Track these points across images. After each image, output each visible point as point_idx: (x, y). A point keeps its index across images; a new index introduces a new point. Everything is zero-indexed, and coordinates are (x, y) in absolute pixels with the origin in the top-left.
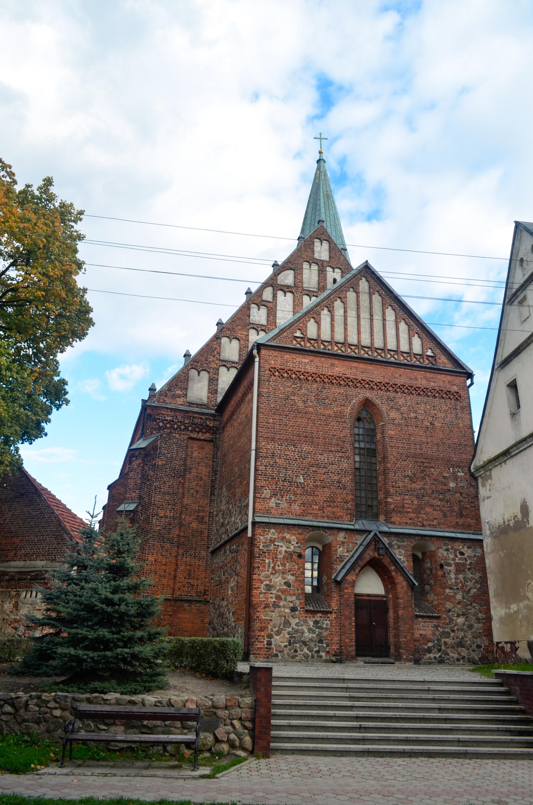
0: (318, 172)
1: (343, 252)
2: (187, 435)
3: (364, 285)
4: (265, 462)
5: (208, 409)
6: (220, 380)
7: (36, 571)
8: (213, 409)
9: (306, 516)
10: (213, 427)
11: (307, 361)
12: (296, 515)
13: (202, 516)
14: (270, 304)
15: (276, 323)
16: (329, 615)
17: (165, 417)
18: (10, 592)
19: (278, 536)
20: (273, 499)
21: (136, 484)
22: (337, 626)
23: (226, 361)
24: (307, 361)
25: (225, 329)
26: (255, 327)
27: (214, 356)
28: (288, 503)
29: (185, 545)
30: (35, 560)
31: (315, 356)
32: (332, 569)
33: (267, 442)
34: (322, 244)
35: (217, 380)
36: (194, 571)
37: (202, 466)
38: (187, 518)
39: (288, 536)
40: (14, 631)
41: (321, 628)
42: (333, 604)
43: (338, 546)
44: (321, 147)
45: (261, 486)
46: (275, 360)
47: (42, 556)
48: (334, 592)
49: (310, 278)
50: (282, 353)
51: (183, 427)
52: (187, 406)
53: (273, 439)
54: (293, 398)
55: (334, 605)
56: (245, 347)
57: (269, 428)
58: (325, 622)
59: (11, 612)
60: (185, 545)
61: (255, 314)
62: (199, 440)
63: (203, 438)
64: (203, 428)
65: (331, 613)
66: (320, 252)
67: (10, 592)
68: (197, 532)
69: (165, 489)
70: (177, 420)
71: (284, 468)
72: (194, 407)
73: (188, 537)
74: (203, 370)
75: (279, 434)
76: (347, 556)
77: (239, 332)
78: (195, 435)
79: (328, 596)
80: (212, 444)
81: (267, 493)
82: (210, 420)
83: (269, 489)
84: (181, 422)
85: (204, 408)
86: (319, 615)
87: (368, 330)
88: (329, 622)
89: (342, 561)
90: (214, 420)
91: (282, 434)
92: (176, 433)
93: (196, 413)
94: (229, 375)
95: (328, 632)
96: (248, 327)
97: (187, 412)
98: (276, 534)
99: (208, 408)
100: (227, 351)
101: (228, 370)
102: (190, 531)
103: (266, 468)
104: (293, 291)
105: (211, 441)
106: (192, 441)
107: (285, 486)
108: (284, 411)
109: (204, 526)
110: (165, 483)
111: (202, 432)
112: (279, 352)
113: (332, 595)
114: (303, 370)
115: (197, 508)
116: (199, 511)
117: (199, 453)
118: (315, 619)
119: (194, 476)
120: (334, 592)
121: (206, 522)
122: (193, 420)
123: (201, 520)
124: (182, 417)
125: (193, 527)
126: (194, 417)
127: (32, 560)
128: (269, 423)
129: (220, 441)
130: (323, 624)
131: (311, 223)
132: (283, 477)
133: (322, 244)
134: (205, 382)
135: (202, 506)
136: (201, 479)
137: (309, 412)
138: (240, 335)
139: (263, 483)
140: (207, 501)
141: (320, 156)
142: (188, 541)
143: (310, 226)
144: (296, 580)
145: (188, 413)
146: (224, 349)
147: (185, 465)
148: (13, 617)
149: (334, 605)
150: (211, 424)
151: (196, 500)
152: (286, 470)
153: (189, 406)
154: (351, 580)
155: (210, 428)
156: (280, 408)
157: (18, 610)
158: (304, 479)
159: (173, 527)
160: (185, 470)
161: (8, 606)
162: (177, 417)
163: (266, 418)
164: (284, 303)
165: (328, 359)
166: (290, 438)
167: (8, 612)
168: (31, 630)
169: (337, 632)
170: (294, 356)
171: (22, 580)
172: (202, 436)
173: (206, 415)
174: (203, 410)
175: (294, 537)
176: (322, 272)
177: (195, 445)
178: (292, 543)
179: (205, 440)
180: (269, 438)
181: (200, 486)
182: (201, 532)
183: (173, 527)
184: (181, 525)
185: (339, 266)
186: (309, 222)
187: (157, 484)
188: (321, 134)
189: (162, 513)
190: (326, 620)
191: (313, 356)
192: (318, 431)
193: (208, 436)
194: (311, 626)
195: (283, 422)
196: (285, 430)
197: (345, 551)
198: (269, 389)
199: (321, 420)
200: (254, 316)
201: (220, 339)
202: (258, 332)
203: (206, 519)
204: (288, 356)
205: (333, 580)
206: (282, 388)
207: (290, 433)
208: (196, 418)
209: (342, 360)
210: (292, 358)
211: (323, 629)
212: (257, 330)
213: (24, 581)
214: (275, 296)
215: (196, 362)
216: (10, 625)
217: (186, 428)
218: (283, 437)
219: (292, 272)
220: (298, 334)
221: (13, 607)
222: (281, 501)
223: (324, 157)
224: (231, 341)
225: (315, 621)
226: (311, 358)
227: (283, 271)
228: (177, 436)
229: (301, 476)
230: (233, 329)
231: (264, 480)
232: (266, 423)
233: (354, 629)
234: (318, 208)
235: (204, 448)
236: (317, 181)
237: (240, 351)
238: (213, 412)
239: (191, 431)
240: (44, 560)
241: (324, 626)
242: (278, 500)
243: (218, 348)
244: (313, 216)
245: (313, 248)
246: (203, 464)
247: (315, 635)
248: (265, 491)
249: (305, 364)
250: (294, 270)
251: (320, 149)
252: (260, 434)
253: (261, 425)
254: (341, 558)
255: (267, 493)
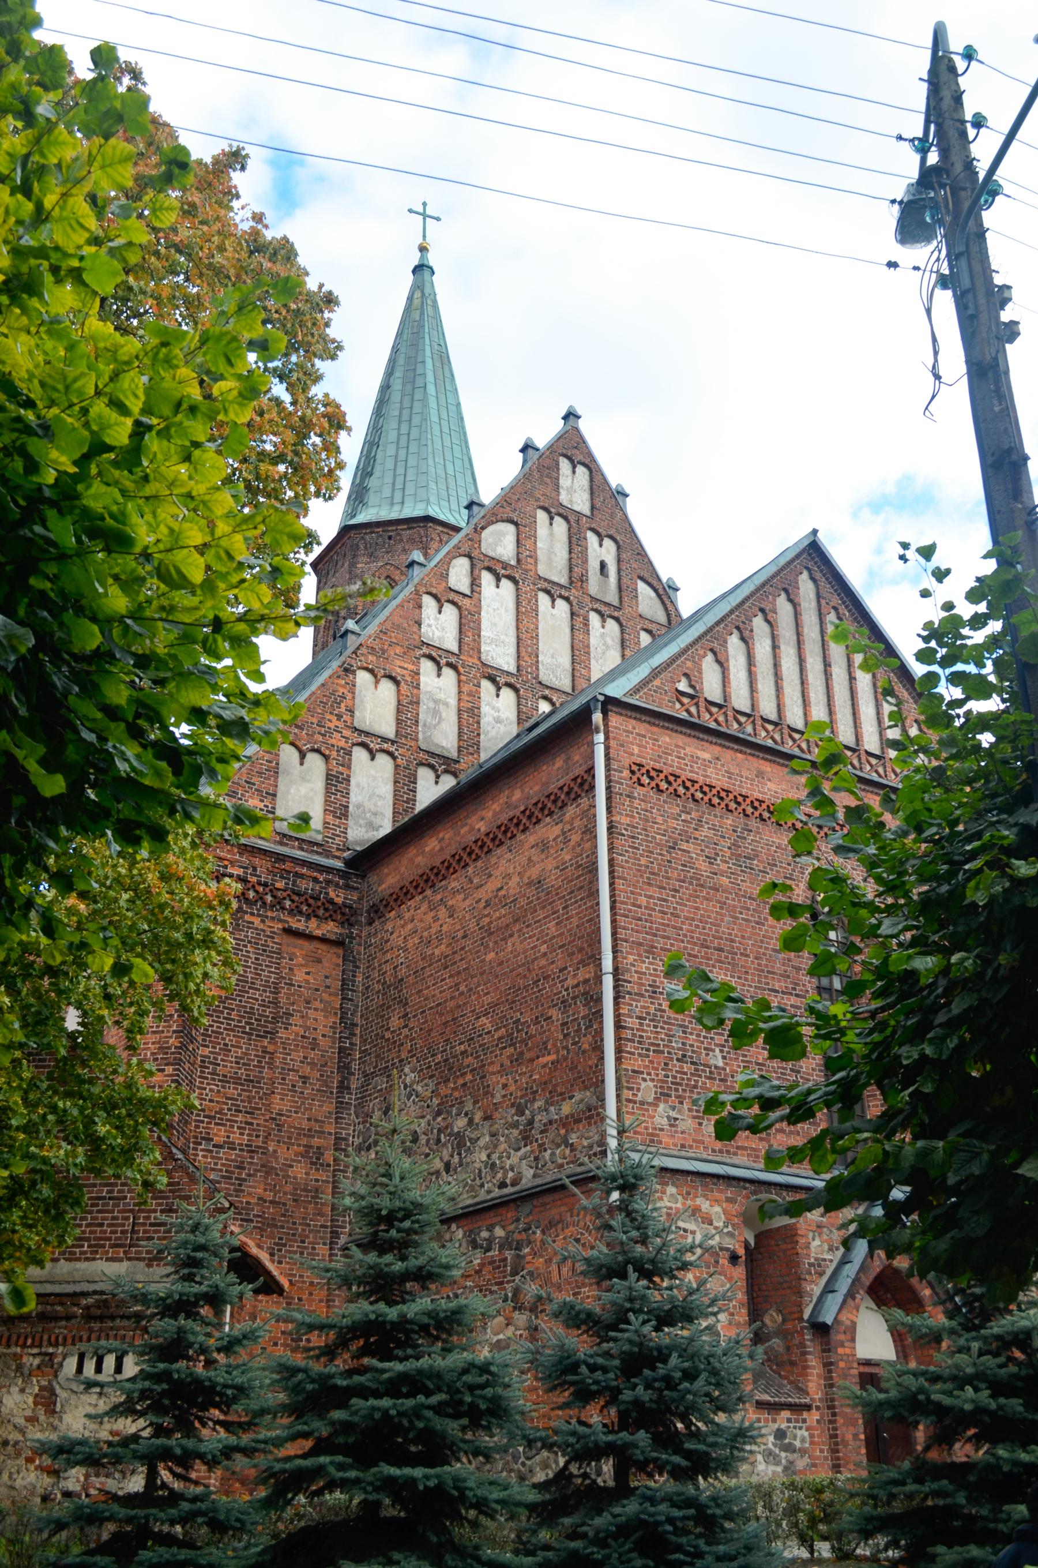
0: (418, 294)
1: (620, 498)
2: (280, 921)
3: (806, 588)
4: (639, 1006)
5: (327, 857)
6: (353, 782)
7: (95, 1292)
8: (338, 858)
9: (735, 1154)
10: (344, 905)
11: (706, 756)
12: (714, 1151)
13: (318, 1148)
14: (466, 603)
15: (479, 652)
16: (805, 1415)
17: (226, 867)
18: (17, 1357)
19: (684, 1204)
20: (662, 1106)
21: (163, 1049)
22: (823, 1443)
23: (367, 734)
24: (706, 756)
25: (363, 650)
26: (434, 654)
27: (339, 717)
28: (694, 1117)
29: (276, 1226)
30: (87, 1259)
31: (724, 746)
32: (800, 1293)
33: (640, 955)
34: (574, 472)
35: (348, 780)
36: (300, 1299)
37: (316, 1009)
38: (282, 1152)
39: (705, 1205)
40: (47, 1480)
41: (789, 1448)
42: (810, 1384)
43: (811, 1234)
44: (424, 236)
45: (634, 1071)
46: (643, 743)
47: (112, 1246)
48: (810, 1353)
49: (551, 552)
50: (655, 729)
51: (269, 898)
52: (275, 842)
53: (651, 950)
54: (684, 846)
55: (815, 1388)
56: (411, 703)
57: (640, 919)
58: (799, 1433)
59: (32, 1420)
60: (276, 1226)
61: (432, 622)
62: (310, 937)
63: (318, 933)
64: (318, 906)
65: (808, 1407)
66: (571, 490)
67: (17, 1357)
68: (305, 1190)
69: (227, 1068)
70: (255, 879)
71: (681, 1026)
72: (293, 847)
73: (284, 1204)
74: (313, 750)
75: (664, 937)
76: (831, 1261)
77: (398, 663)
78: (298, 924)
79: (793, 1363)
80: (341, 952)
81: (647, 1090)
82: (337, 885)
83: (652, 1080)
84: (266, 885)
85: (317, 853)
86: (786, 1414)
87: (823, 699)
88: (806, 1434)
89: (821, 1274)
90: (347, 887)
91: (669, 938)
92: (252, 914)
93: (304, 863)
94: (372, 772)
95: (806, 1460)
96: (419, 652)
97: (281, 858)
98: (680, 1197)
99: (328, 854)
100: (369, 706)
101: (373, 759)
102: (289, 1188)
103: (641, 1024)
104: (517, 576)
105: (339, 943)
106: (292, 940)
107: (685, 1073)
108: (668, 878)
109: (323, 1176)
110: (226, 1050)
111: (316, 916)
112: (647, 726)
113: (806, 1361)
114: (701, 780)
115: (305, 1124)
116: (310, 1133)
117: (308, 973)
118: (776, 1426)
119: (297, 1034)
120: (810, 1353)
121: (329, 1165)
122: (294, 881)
123: (314, 1157)
124: (270, 872)
125: (295, 1178)
126: (297, 875)
127: (79, 1260)
128: (640, 907)
129: (360, 945)
130: (795, 1438)
131: (400, 416)
132: (679, 1049)
133: (574, 472)
134: (318, 784)
135: (316, 1121)
136: (314, 1045)
137: (721, 886)
138: (399, 670)
139: (638, 1063)
140: (329, 1107)
141: (422, 257)
142: (284, 1215)
143: (400, 422)
144: (730, 1324)
145: (284, 861)
146: (362, 701)
147: (275, 1003)
148: (39, 1436)
149: (815, 1388)
150: (338, 896)
151: (303, 1103)
152: (684, 1032)
153: (281, 843)
154: (848, 1323)
155: (338, 908)
156: (660, 870)
157: (54, 1412)
158: (724, 1058)
159: (249, 1175)
160: (276, 1019)
161: (17, 1401)
162: (255, 869)
163: (632, 893)
164: (496, 605)
165: (750, 758)
166: (685, 948)
167: (20, 1421)
168: (107, 1476)
169: (826, 1459)
170: (680, 740)
171: (56, 1318)
172: (318, 927)
173: (328, 873)
174: (316, 857)
175: (717, 1209)
176: (575, 543)
177: (300, 949)
178: (715, 1224)
179: (323, 940)
180: (641, 944)
181: (313, 1064)
182: (317, 1191)
183: (249, 1175)
184: (268, 1170)
185: (611, 532)
186: (397, 413)
187: (206, 1051)
188: (425, 204)
189: (219, 1134)
190: (801, 1428)
191: (720, 745)
192: (743, 937)
193: (330, 929)
194: (770, 1446)
195: (668, 907)
196: (675, 927)
197: (826, 1247)
198: (633, 817)
199: (748, 909)
200: (430, 626)
201: (354, 672)
202: (440, 669)
203: (329, 1156)
204: (667, 739)
205: (808, 1321)
206: (660, 820)
207: (685, 936)
208: (302, 876)
209: (779, 764)
210: (677, 746)
211: (794, 1451)
212: (437, 663)
213: (64, 1323)
214: (475, 582)
215: (297, 726)
216: (29, 1460)
217: (278, 903)
218: (672, 945)
219: (511, 528)
220: (683, 686)
221: (36, 1404)
222: (680, 1111)
223: (432, 260)
224: (377, 682)
225: (778, 1430)
226: (717, 749)
227: (493, 523)
228: (257, 921)
229: (717, 1050)
230: (384, 651)
231: (640, 1055)
232: (634, 905)
233: (863, 1451)
234: (419, 382)
235: (319, 961)
236: (416, 315)
237: (398, 711)
238: (339, 864)
239: (291, 912)
240: (121, 1260)
241: (797, 1444)
242: (673, 1108)
243: (349, 696)
244: (407, 399)
245: (558, 479)
246: (317, 1004)
247: (779, 1469)
248: (643, 1085)
249: (707, 764)
250: (516, 524)
251: (421, 240)
252: (622, 934)
253: (621, 908)
254: (819, 1266)
255: (647, 1090)
